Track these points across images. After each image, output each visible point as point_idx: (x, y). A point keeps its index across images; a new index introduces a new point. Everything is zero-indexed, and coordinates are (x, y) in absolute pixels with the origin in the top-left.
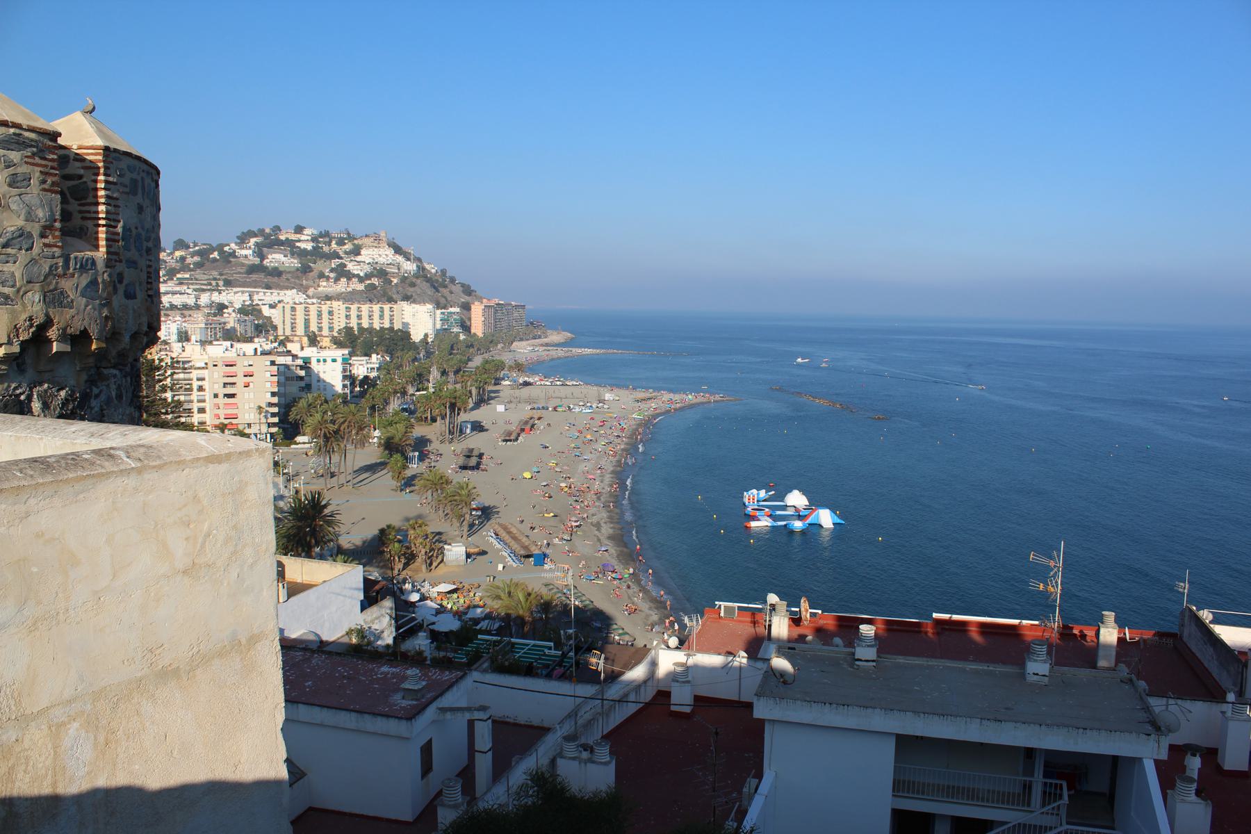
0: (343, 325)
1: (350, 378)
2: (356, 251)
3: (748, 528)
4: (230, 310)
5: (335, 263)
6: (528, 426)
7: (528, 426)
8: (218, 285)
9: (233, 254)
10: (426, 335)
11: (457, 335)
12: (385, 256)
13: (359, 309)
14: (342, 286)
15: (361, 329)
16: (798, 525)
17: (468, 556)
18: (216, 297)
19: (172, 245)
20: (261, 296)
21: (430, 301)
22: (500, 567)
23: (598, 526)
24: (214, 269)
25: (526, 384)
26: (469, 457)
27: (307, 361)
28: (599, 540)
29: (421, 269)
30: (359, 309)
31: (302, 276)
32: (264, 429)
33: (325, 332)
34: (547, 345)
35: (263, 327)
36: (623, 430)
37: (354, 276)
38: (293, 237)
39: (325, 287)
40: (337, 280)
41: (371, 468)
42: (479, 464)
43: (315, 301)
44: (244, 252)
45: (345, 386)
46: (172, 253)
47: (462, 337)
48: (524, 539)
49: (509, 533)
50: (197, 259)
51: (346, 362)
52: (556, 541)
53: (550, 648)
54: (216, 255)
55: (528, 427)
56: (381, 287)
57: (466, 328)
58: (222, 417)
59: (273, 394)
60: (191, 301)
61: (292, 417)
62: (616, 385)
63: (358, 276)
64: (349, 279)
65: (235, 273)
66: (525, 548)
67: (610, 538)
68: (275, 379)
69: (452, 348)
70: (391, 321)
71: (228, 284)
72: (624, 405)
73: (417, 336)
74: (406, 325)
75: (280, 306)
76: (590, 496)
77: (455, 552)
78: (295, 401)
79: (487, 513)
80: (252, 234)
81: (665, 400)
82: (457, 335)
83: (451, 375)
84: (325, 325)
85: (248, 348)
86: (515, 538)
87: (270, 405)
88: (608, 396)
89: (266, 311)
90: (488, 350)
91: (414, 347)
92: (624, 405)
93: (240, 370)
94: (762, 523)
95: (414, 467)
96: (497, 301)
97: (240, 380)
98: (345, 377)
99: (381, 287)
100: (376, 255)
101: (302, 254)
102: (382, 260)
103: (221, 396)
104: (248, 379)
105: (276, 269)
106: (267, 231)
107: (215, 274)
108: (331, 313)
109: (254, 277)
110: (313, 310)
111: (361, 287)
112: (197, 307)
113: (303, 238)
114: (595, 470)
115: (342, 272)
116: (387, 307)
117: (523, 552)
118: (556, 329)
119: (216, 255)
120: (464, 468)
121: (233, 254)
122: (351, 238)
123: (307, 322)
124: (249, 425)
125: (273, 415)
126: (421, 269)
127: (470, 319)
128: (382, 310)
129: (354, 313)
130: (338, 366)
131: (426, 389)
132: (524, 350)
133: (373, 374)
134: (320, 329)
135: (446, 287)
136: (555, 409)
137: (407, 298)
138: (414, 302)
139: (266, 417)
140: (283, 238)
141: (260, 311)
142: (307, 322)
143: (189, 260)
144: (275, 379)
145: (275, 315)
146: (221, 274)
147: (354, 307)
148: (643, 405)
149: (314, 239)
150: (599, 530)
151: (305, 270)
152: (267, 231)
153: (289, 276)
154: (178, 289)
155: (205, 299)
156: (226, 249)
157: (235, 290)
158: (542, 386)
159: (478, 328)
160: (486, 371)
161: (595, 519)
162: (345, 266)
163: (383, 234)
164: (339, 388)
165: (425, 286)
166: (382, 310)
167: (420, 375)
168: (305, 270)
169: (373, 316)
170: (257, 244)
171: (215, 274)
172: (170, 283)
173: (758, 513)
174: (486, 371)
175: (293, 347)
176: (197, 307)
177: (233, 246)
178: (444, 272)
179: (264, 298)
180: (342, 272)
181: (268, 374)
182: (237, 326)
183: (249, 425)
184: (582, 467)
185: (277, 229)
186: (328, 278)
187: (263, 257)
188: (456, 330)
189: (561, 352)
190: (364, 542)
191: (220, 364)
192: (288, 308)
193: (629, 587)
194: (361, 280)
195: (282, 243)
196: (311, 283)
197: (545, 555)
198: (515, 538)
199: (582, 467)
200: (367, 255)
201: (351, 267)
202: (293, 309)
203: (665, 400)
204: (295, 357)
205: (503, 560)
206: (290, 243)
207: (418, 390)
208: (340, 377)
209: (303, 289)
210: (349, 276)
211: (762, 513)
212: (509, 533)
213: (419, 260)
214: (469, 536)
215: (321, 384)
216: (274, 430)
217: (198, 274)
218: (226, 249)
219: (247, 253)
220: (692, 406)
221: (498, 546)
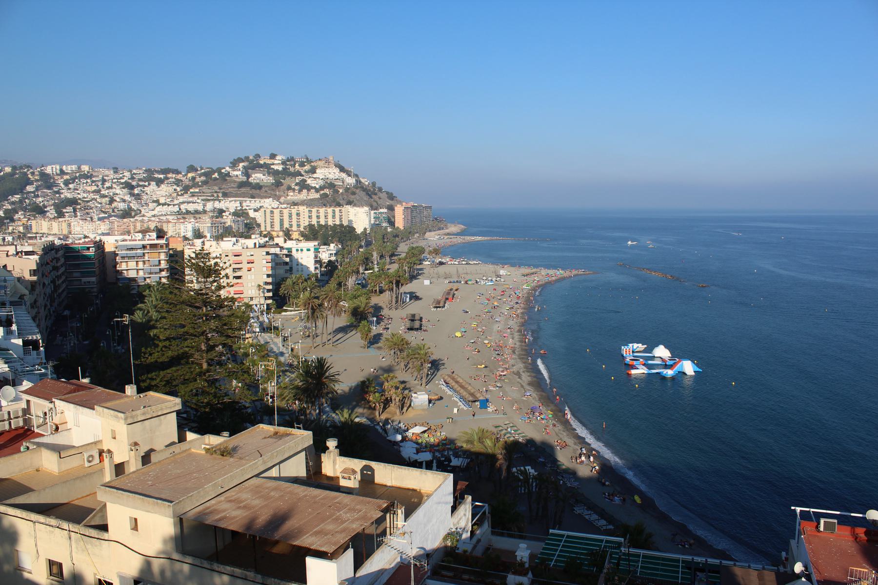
0: (307, 224)
1: (318, 262)
2: (313, 171)
3: (629, 375)
4: (227, 213)
5: (298, 179)
6: (450, 296)
7: (450, 296)
8: (218, 196)
9: (228, 174)
10: (365, 229)
11: (386, 228)
12: (333, 173)
13: (318, 212)
14: (304, 195)
15: (320, 226)
16: (669, 373)
17: (430, 401)
18: (217, 205)
19: (186, 169)
20: (248, 203)
21: (367, 205)
22: (455, 410)
23: (518, 374)
24: (216, 185)
25: (441, 263)
26: (412, 320)
27: (290, 250)
28: (522, 386)
29: (358, 182)
30: (318, 212)
31: (276, 189)
32: (262, 301)
33: (295, 228)
34: (448, 234)
35: (249, 228)
36: (518, 298)
37: (312, 188)
38: (269, 162)
39: (292, 196)
40: (300, 191)
41: (343, 330)
42: (421, 325)
43: (285, 206)
44: (236, 173)
45: (316, 268)
46: (186, 175)
47: (389, 230)
48: (470, 388)
49: (457, 382)
50: (203, 178)
51: (317, 251)
52: (491, 388)
53: (619, 545)
54: (216, 175)
55: (451, 297)
56: (332, 196)
57: (392, 223)
58: (232, 293)
59: (268, 276)
60: (200, 208)
61: (281, 292)
62: (504, 261)
63: (315, 188)
64: (309, 190)
65: (230, 188)
66: (472, 395)
67: (530, 384)
68: (270, 265)
69: (384, 237)
70: (341, 219)
71: (225, 195)
72: (519, 280)
73: (359, 230)
74: (350, 221)
75: (262, 210)
76: (507, 351)
77: (420, 398)
78: (284, 280)
79: (436, 365)
80: (240, 160)
81: (544, 275)
82: (386, 228)
83: (388, 258)
84: (294, 223)
85: (250, 243)
86: (462, 387)
87: (267, 283)
88: (502, 272)
89: (252, 214)
90: (408, 239)
91: (357, 237)
92: (519, 280)
93: (244, 259)
94: (640, 371)
95: (375, 330)
96: (412, 203)
97: (245, 266)
98: (316, 262)
99: (332, 196)
100: (327, 172)
101: (276, 173)
102: (331, 176)
103: (231, 277)
104: (250, 265)
105: (258, 184)
106: (251, 158)
107: (216, 188)
108: (298, 215)
109: (243, 190)
110: (286, 212)
111: (317, 196)
112: (205, 212)
113: (276, 162)
114: (506, 329)
115: (303, 186)
116: (337, 210)
117: (471, 399)
118: (453, 223)
119: (216, 175)
120: (411, 329)
121: (228, 174)
122: (309, 161)
123: (282, 221)
124: (252, 298)
125: (269, 291)
126: (358, 182)
127: (394, 217)
128: (334, 212)
129: (314, 215)
130: (312, 254)
131: (372, 269)
132: (433, 238)
133: (333, 258)
134: (291, 226)
135: (376, 194)
136: (466, 282)
137: (349, 203)
138: (355, 205)
139: (264, 292)
140: (262, 162)
141: (247, 214)
142: (282, 221)
143: (198, 179)
144: (270, 265)
145: (259, 217)
146: (220, 189)
147: (314, 210)
148: (528, 279)
149: (284, 163)
150: (520, 378)
151: (278, 184)
152: (251, 158)
153: (267, 189)
154: (191, 199)
155: (209, 206)
156: (223, 171)
157: (230, 199)
158: (453, 266)
159: (400, 223)
160: (414, 255)
161: (515, 369)
162: (306, 181)
163: (331, 158)
164: (312, 267)
165: (363, 194)
166: (334, 212)
167: (367, 259)
168: (278, 184)
169: (328, 216)
170: (244, 167)
171: (216, 188)
172: (186, 196)
173: (635, 363)
174: (414, 255)
175: (280, 241)
176: (205, 212)
177: (228, 169)
178: (374, 184)
179: (250, 204)
180: (303, 186)
181: (264, 261)
182: (233, 225)
183: (252, 298)
184: (496, 327)
185: (258, 156)
186: (294, 190)
187: (248, 176)
188: (384, 225)
189: (459, 240)
190: (350, 389)
191: (230, 255)
192: (268, 212)
193: (554, 425)
194: (317, 191)
195: (261, 166)
196: (282, 193)
197: (487, 400)
198: (462, 387)
199: (496, 327)
200: (321, 173)
201: (309, 181)
202: (272, 212)
203: (544, 275)
204: (282, 248)
205: (455, 404)
206: (267, 166)
207: (366, 270)
208: (313, 261)
209: (277, 198)
210: (309, 188)
211: (638, 362)
212: (457, 382)
213: (356, 176)
214: (427, 383)
215: (300, 267)
216: (270, 301)
217: (205, 189)
218: (223, 171)
219: (237, 173)
220: (563, 279)
221: (449, 393)
